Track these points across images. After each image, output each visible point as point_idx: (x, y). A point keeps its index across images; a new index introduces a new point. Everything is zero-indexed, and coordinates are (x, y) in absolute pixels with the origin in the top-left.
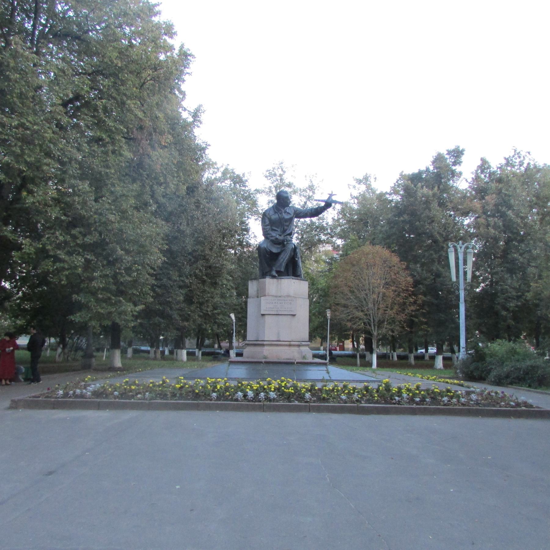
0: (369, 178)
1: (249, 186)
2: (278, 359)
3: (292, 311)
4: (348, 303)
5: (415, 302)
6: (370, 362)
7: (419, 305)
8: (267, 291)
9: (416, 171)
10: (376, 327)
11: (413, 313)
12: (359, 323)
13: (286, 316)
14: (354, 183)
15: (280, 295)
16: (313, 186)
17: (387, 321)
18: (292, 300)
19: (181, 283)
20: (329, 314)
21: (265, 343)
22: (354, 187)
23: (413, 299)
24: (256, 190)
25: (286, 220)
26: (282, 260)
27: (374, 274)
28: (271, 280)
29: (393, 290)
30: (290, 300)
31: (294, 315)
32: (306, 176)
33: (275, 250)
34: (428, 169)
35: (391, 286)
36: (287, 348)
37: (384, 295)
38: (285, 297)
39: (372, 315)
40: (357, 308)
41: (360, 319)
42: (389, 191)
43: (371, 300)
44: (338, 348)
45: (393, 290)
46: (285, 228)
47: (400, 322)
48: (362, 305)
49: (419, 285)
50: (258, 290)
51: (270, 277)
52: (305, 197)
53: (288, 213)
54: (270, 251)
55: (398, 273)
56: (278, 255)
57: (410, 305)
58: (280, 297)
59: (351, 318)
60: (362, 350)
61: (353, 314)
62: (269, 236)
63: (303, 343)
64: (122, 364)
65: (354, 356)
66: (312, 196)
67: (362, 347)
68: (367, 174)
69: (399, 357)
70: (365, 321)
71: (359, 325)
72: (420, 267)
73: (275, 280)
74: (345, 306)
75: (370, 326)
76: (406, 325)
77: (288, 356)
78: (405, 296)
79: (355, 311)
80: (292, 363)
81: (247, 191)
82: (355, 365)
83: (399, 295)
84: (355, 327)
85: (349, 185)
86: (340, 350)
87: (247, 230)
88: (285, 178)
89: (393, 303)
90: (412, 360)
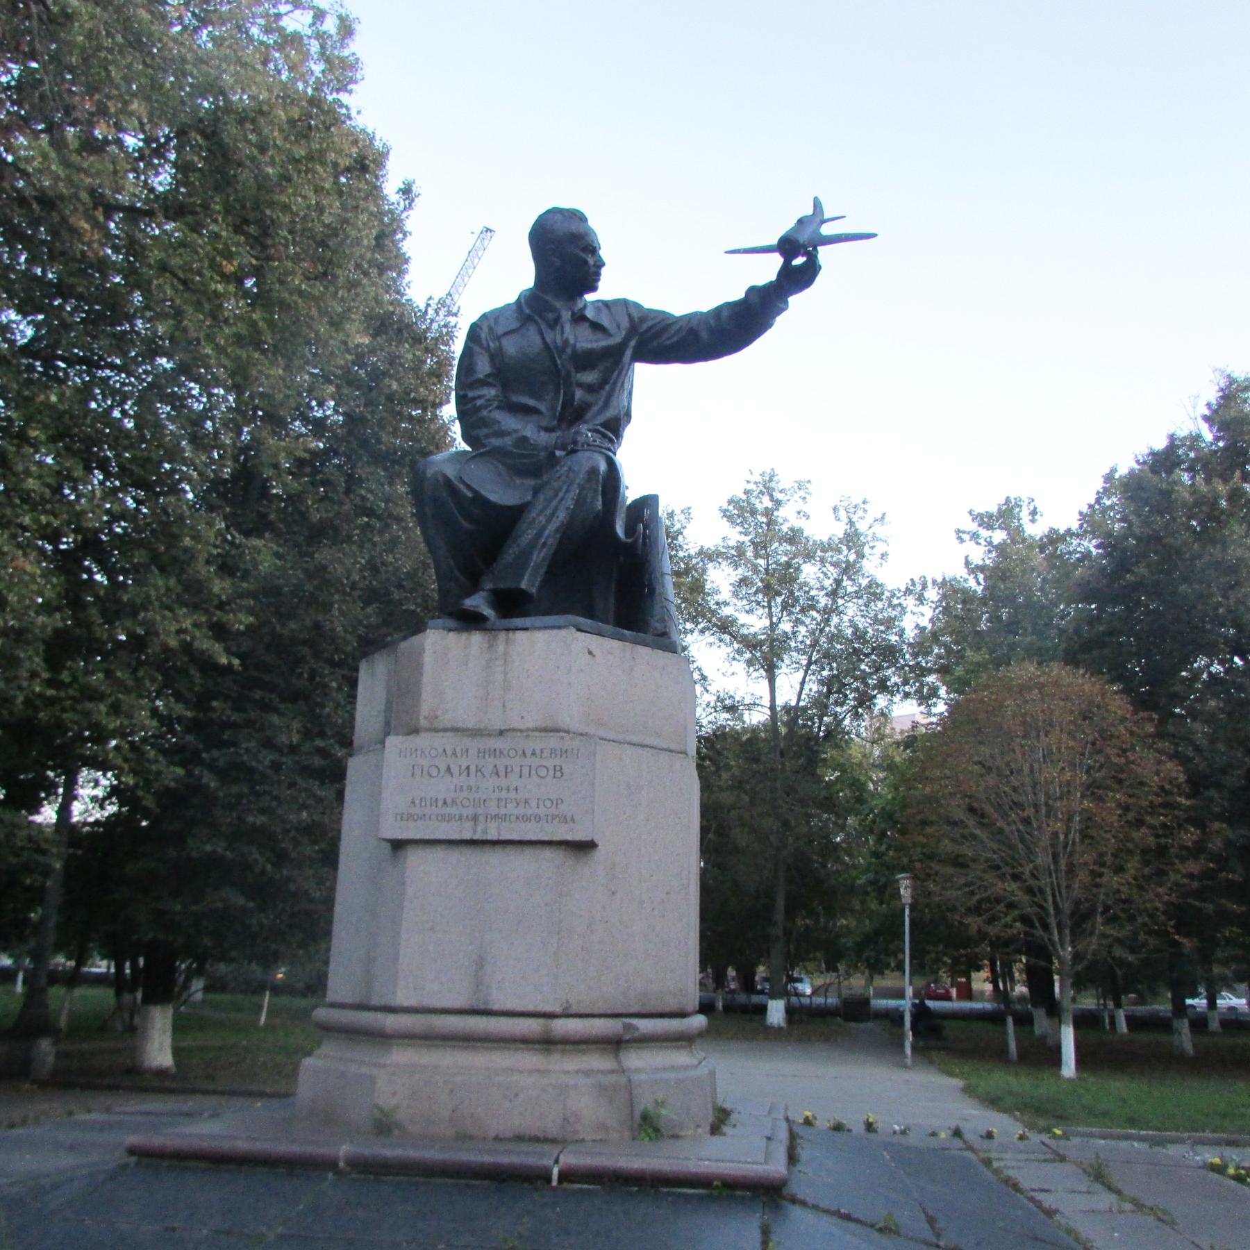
2: (464, 1138)
5: (1197, 850)
6: (1050, 1041)
8: (426, 707)
9: (1161, 444)
10: (1067, 931)
12: (1009, 919)
13: (529, 852)
14: (974, 527)
15: (499, 725)
16: (857, 534)
17: (1107, 909)
18: (564, 753)
19: (318, 761)
20: (905, 891)
21: (392, 1022)
22: (975, 536)
24: (701, 552)
25: (585, 360)
26: (530, 533)
27: (1048, 755)
29: (1119, 805)
31: (584, 847)
32: (835, 509)
33: (500, 493)
34: (1197, 438)
35: (1112, 790)
36: (530, 1059)
37: (1088, 818)
38: (526, 732)
39: (1049, 891)
40: (998, 867)
41: (1011, 906)
42: (1075, 526)
43: (1045, 841)
44: (954, 992)
45: (1119, 805)
46: (579, 394)
49: (1207, 788)
51: (451, 623)
52: (835, 565)
53: (596, 327)
54: (476, 493)
56: (508, 519)
57: (1183, 859)
58: (501, 733)
59: (980, 902)
60: (1022, 999)
61: (986, 889)
62: (485, 431)
63: (645, 1026)
64: (177, 1052)
65: (995, 1018)
66: (855, 562)
67: (1021, 989)
68: (1008, 500)
69: (1131, 1020)
70: (1029, 910)
71: (1006, 926)
73: (476, 639)
74: (958, 862)
75: (1046, 927)
78: (1164, 825)
79: (990, 877)
81: (682, 559)
82: (999, 1055)
83: (1139, 823)
84: (992, 931)
85: (958, 531)
90: (1185, 1038)
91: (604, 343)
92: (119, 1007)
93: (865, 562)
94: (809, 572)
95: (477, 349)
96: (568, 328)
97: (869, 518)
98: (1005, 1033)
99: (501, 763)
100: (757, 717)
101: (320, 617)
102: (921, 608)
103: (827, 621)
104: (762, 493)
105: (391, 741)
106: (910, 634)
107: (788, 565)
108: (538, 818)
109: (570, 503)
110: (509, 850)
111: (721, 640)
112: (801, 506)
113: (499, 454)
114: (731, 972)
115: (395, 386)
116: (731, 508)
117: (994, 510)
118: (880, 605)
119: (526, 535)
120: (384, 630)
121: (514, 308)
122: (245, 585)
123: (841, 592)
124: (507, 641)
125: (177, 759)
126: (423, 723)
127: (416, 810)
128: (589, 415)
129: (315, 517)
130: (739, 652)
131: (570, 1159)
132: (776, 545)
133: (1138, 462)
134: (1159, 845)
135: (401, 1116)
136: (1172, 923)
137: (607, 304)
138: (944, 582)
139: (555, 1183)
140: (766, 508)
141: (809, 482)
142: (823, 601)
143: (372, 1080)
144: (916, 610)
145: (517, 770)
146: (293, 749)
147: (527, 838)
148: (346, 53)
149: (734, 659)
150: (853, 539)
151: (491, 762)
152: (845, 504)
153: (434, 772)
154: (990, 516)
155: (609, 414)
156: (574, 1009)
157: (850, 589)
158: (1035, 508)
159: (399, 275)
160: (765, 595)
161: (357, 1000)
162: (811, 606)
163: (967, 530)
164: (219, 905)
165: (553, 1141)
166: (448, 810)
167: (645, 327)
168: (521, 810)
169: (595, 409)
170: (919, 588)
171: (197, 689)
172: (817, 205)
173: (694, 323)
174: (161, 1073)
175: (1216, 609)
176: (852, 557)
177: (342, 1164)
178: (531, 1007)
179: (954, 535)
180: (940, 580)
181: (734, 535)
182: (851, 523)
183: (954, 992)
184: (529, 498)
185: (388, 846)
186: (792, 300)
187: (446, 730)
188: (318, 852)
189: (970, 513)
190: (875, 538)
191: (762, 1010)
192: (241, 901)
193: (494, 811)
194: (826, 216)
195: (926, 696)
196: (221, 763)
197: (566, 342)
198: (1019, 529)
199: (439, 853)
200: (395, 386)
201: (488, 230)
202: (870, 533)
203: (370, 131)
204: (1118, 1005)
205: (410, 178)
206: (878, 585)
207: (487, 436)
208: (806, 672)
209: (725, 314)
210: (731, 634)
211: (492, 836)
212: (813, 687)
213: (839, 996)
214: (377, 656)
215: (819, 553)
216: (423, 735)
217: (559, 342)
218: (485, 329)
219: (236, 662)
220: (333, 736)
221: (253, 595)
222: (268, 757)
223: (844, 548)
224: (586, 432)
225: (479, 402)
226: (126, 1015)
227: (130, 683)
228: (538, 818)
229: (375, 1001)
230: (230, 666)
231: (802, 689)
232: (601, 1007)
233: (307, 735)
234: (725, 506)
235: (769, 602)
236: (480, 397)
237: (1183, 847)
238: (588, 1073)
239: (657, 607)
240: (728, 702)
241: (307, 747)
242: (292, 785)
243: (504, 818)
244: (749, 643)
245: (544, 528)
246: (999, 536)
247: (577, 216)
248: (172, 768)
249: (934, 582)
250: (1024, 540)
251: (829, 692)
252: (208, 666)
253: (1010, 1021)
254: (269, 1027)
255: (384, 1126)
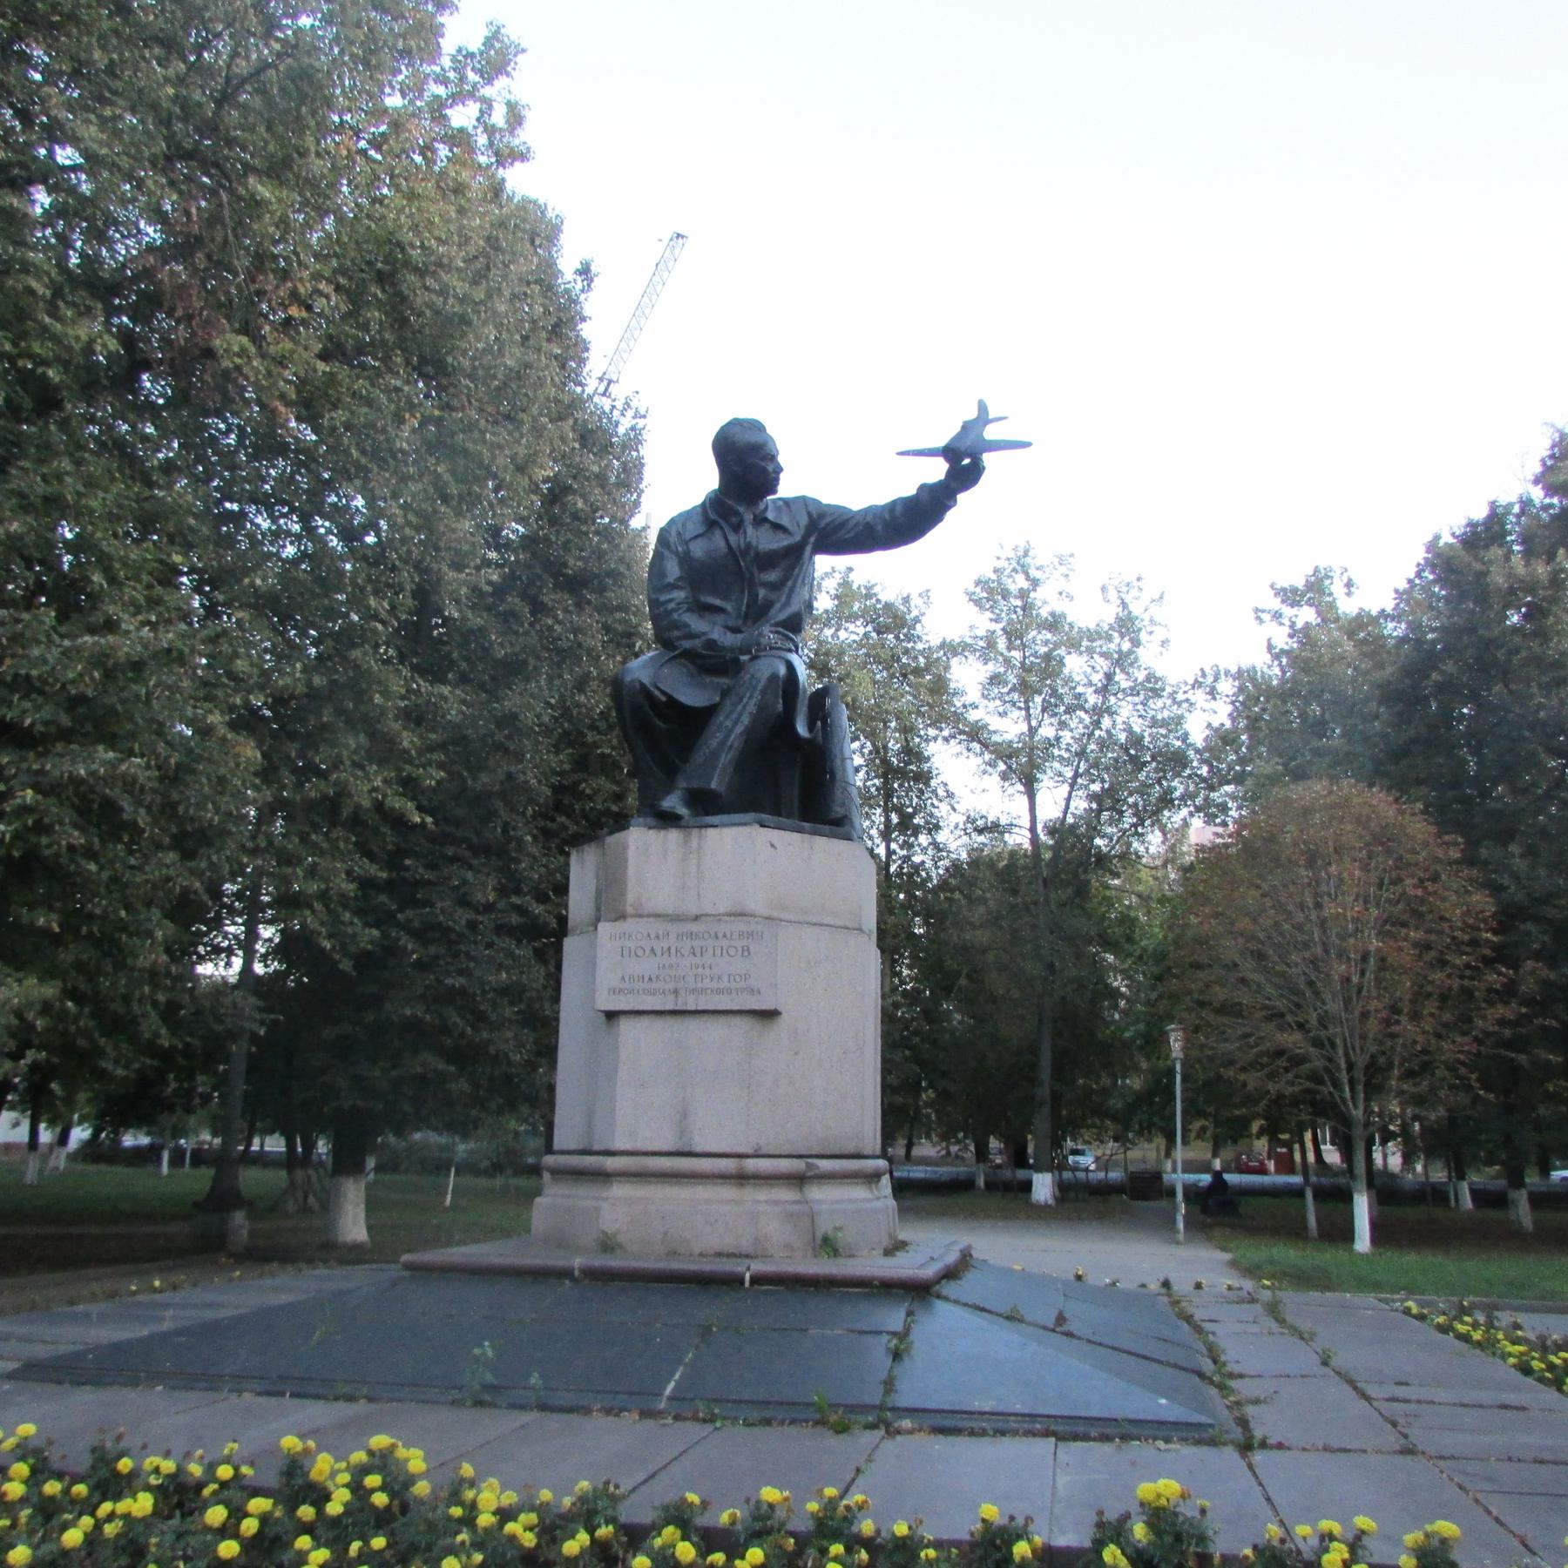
0: (1327, 582)
1: (925, 638)
2: (673, 1253)
3: (753, 991)
4: (1244, 997)
5: (1509, 992)
7: (1529, 1002)
8: (631, 897)
9: (1480, 513)
10: (1360, 1088)
11: (1508, 1033)
13: (722, 1019)
14: (1275, 604)
15: (695, 911)
17: (1401, 1065)
19: (515, 919)
20: (1176, 1043)
21: (611, 1163)
22: (1277, 616)
23: (1500, 974)
24: (943, 645)
25: (768, 560)
28: (652, 833)
29: (1415, 945)
30: (741, 934)
31: (770, 1015)
32: (1104, 589)
33: (692, 696)
36: (727, 1192)
38: (718, 918)
42: (1389, 606)
44: (1271, 1165)
45: (1415, 945)
46: (762, 593)
47: (1451, 1068)
48: (1298, 1006)
50: (599, 892)
51: (650, 821)
52: (1105, 655)
53: (777, 527)
54: (670, 698)
55: (1435, 878)
56: (710, 712)
57: (1491, 1003)
58: (697, 918)
62: (676, 633)
63: (825, 1165)
66: (1130, 652)
68: (1316, 570)
69: (1477, 1195)
72: (1522, 856)
73: (673, 835)
75: (1336, 1084)
76: (1478, 1080)
77: (712, 1239)
78: (1468, 966)
79: (1269, 1028)
80: (732, 1282)
81: (922, 652)
82: (1295, 1231)
85: (1257, 610)
86: (1278, 1171)
87: (924, 778)
88: (1038, 603)
89: (1420, 996)
90: (1523, 1213)
91: (785, 543)
92: (292, 1184)
93: (1140, 651)
94: (1075, 664)
95: (666, 553)
96: (750, 530)
97: (1145, 599)
98: (1304, 1206)
99: (697, 944)
100: (1020, 839)
101: (512, 769)
102: (1213, 704)
103: (1097, 724)
104: (1015, 570)
105: (601, 926)
106: (1198, 736)
107: (1048, 657)
108: (729, 991)
109: (752, 708)
110: (705, 1018)
111: (969, 750)
112: (1062, 585)
113: (689, 655)
114: (994, 1143)
115: (580, 504)
116: (978, 590)
117: (1300, 584)
118: (1160, 703)
119: (713, 738)
120: (576, 777)
121: (698, 518)
122: (433, 736)
123: (1113, 689)
124: (700, 837)
125: (371, 919)
126: (630, 910)
127: (626, 985)
128: (772, 612)
129: (501, 653)
130: (992, 764)
131: (758, 1267)
132: (1033, 633)
133: (1453, 535)
134: (1463, 989)
135: (621, 1238)
136: (1474, 1076)
137: (787, 502)
138: (1240, 672)
139: (747, 1284)
140: (1021, 589)
141: (1072, 555)
142: (1092, 699)
143: (597, 1209)
144: (1207, 706)
145: (711, 950)
146: (489, 908)
147: (721, 1008)
148: (516, 142)
149: (985, 772)
150: (1126, 625)
151: (687, 945)
152: (1115, 582)
153: (640, 952)
154: (1294, 590)
155: (793, 609)
156: (765, 1151)
157: (1125, 684)
158: (1350, 580)
159: (579, 365)
160: (1022, 693)
161: (580, 1147)
162: (1078, 705)
163: (1267, 608)
164: (419, 1070)
165: (747, 1256)
166: (655, 985)
167: (823, 524)
168: (714, 985)
169: (778, 606)
170: (1210, 679)
171: (390, 847)
172: (982, 407)
173: (869, 518)
174: (357, 1247)
175: (1537, 712)
176: (1126, 646)
177: (577, 1273)
178: (727, 1150)
179: (1253, 615)
180: (1234, 670)
181: (983, 623)
182: (1124, 605)
183: (1271, 1165)
184: (717, 699)
185: (602, 1016)
186: (961, 497)
187: (649, 916)
188: (518, 1013)
189: (1272, 586)
190: (1152, 621)
191: (1027, 1186)
192: (441, 1066)
193: (692, 985)
194: (991, 416)
195: (1210, 812)
196: (416, 924)
197: (749, 546)
198: (1332, 606)
199: (645, 1022)
200: (580, 504)
201: (679, 236)
202: (1146, 617)
203: (541, 202)
204: (1461, 1177)
205: (588, 258)
206: (1158, 679)
207: (679, 638)
208: (1072, 786)
209: (899, 508)
210: (980, 742)
211: (691, 1007)
212: (1080, 805)
213: (1126, 1170)
214: (586, 847)
215: (1085, 643)
216: (629, 920)
217: (743, 545)
218: (673, 533)
219: (429, 820)
220: (529, 892)
221: (442, 746)
222: (463, 916)
223: (1116, 635)
224: (769, 635)
225: (672, 606)
226: (300, 1194)
227: (325, 845)
228: (729, 991)
229: (596, 1147)
230: (423, 824)
231: (1067, 807)
232: (786, 1150)
233: (502, 891)
234: (971, 588)
235: (1026, 702)
236: (671, 600)
237: (1490, 990)
238: (776, 1203)
239: (838, 793)
240: (980, 823)
241: (501, 905)
242: (490, 946)
243: (703, 991)
244: (1003, 753)
245: (731, 731)
246: (1307, 615)
247: (756, 426)
248: (367, 931)
249: (1227, 673)
250: (1337, 620)
251: (1100, 811)
252: (398, 822)
253: (1362, 1207)
254: (454, 1206)
255: (608, 1245)
